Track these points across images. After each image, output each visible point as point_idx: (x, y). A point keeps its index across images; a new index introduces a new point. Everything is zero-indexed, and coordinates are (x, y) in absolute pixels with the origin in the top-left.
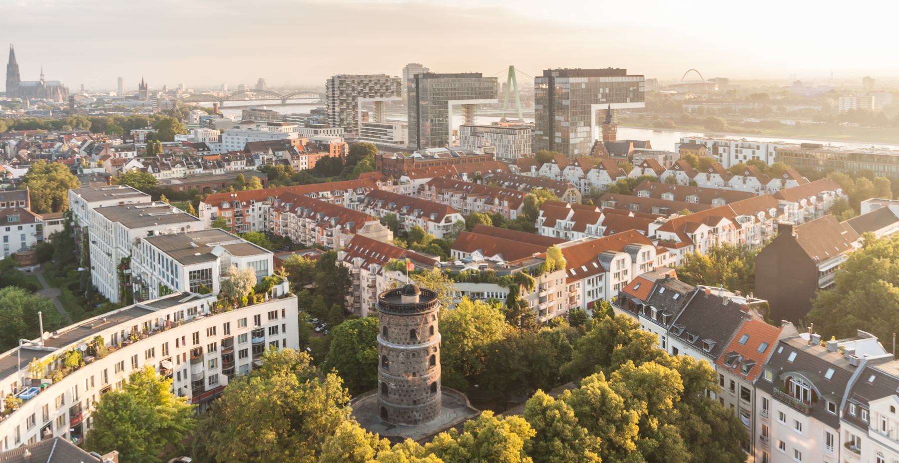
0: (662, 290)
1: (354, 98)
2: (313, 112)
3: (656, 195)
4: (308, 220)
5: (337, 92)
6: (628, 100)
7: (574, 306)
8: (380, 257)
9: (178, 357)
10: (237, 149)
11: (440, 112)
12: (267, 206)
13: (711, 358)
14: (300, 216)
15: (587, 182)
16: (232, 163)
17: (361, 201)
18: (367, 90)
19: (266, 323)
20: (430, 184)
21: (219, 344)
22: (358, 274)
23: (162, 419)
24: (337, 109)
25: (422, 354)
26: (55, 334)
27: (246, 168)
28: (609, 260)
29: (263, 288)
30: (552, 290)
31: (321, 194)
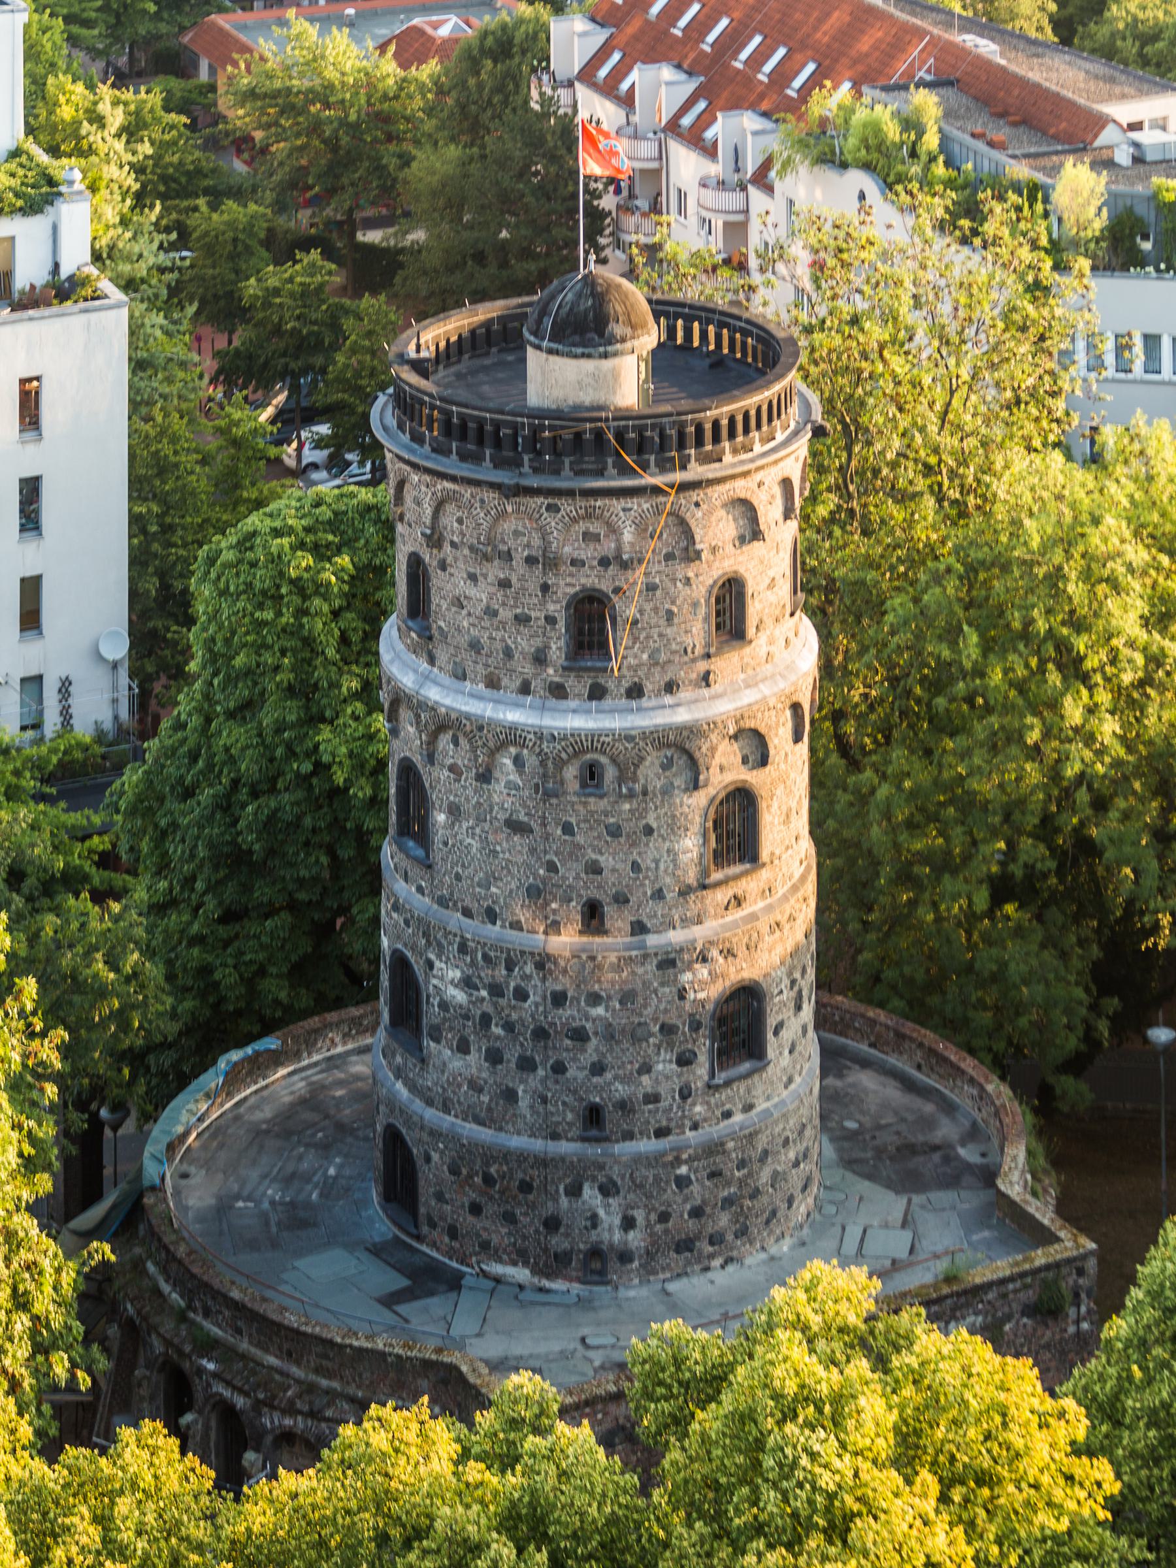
8: (782, 76)
22: (654, 176)
25: (650, 772)
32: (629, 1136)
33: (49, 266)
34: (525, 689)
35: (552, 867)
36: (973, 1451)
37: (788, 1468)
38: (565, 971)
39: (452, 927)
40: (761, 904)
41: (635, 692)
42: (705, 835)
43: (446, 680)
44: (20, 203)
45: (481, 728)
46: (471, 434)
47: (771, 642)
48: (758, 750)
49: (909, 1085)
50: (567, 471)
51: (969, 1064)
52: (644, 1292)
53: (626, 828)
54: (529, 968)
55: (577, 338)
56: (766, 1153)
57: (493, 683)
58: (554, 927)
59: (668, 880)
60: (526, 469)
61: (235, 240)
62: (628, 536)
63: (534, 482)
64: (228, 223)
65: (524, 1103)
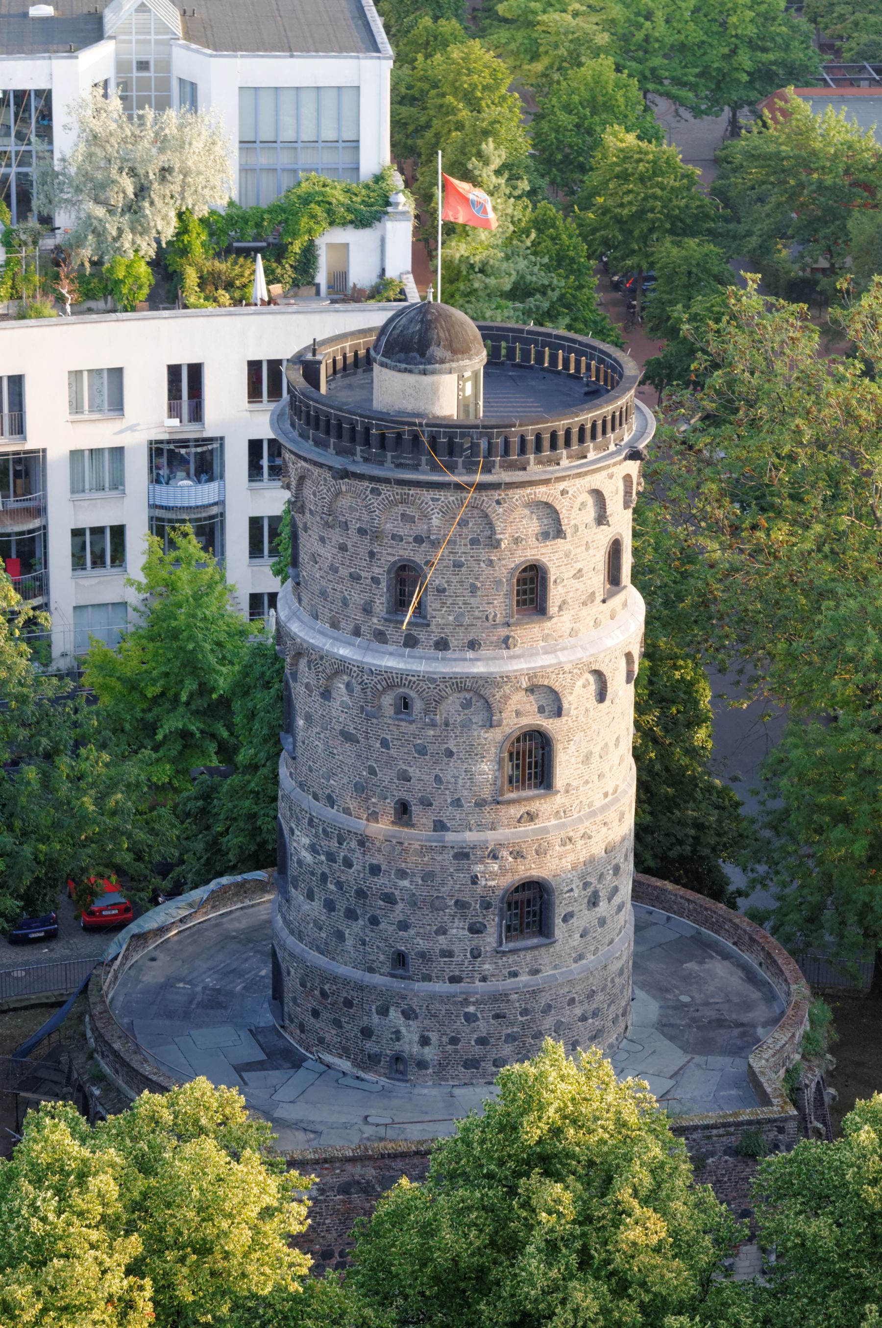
25: (451, 706)
32: (427, 978)
33: (378, 271)
34: (357, 632)
35: (372, 771)
38: (379, 850)
39: (305, 806)
40: (554, 822)
41: (442, 645)
42: (500, 762)
43: (306, 617)
44: (351, 217)
45: (322, 658)
46: (322, 425)
47: (576, 620)
49: (751, 977)
50: (389, 464)
52: (435, 1092)
53: (431, 748)
54: (354, 844)
55: (402, 356)
56: (549, 1007)
57: (335, 625)
58: (373, 816)
59: (466, 793)
60: (358, 458)
61: (690, 273)
62: (435, 522)
63: (358, 469)
64: (686, 259)
65: (349, 942)
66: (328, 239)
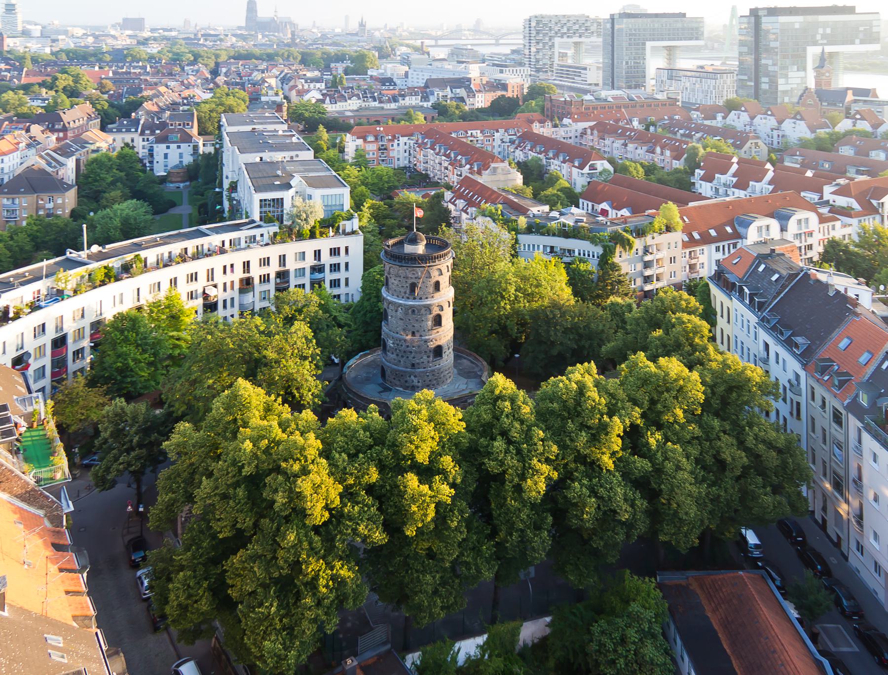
0: (762, 267)
1: (551, 38)
2: (513, 52)
3: (862, 152)
4: (444, 158)
5: (534, 32)
6: (857, 41)
7: (694, 276)
9: (225, 284)
10: (416, 85)
11: (637, 53)
12: (412, 142)
13: (800, 361)
14: (437, 154)
15: (781, 133)
16: (407, 98)
17: (512, 142)
18: (565, 30)
19: (326, 259)
20: (592, 128)
21: (273, 276)
22: (460, 217)
23: (176, 346)
24: (533, 49)
25: (423, 311)
26: (104, 248)
27: (421, 104)
28: (747, 225)
29: (330, 224)
30: (664, 254)
31: (469, 132)
36: (443, 419)
37: (408, 421)
41: (421, 299)
48: (441, 308)
49: (472, 362)
51: (481, 359)
66: (342, 223)
